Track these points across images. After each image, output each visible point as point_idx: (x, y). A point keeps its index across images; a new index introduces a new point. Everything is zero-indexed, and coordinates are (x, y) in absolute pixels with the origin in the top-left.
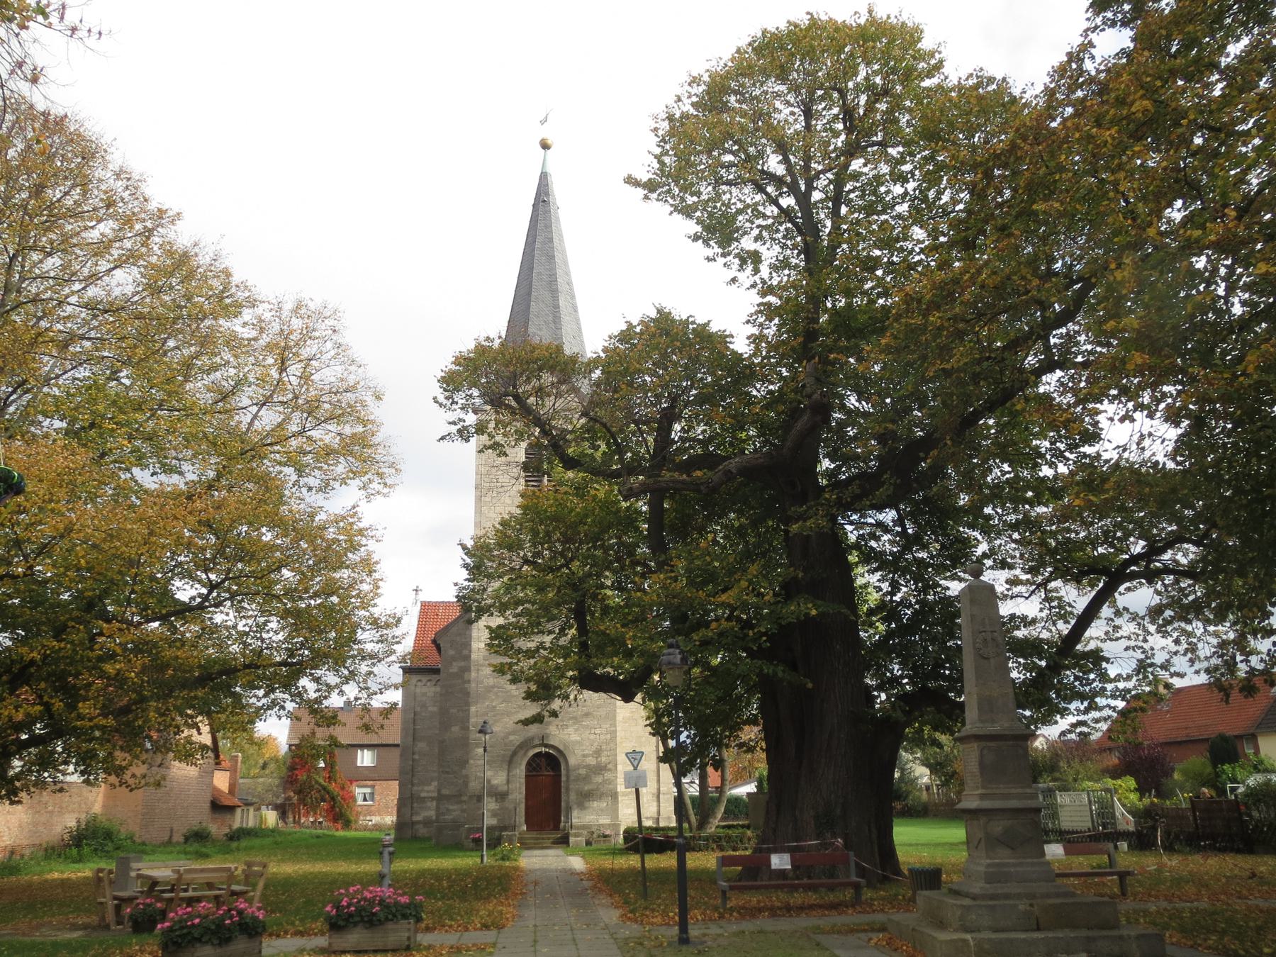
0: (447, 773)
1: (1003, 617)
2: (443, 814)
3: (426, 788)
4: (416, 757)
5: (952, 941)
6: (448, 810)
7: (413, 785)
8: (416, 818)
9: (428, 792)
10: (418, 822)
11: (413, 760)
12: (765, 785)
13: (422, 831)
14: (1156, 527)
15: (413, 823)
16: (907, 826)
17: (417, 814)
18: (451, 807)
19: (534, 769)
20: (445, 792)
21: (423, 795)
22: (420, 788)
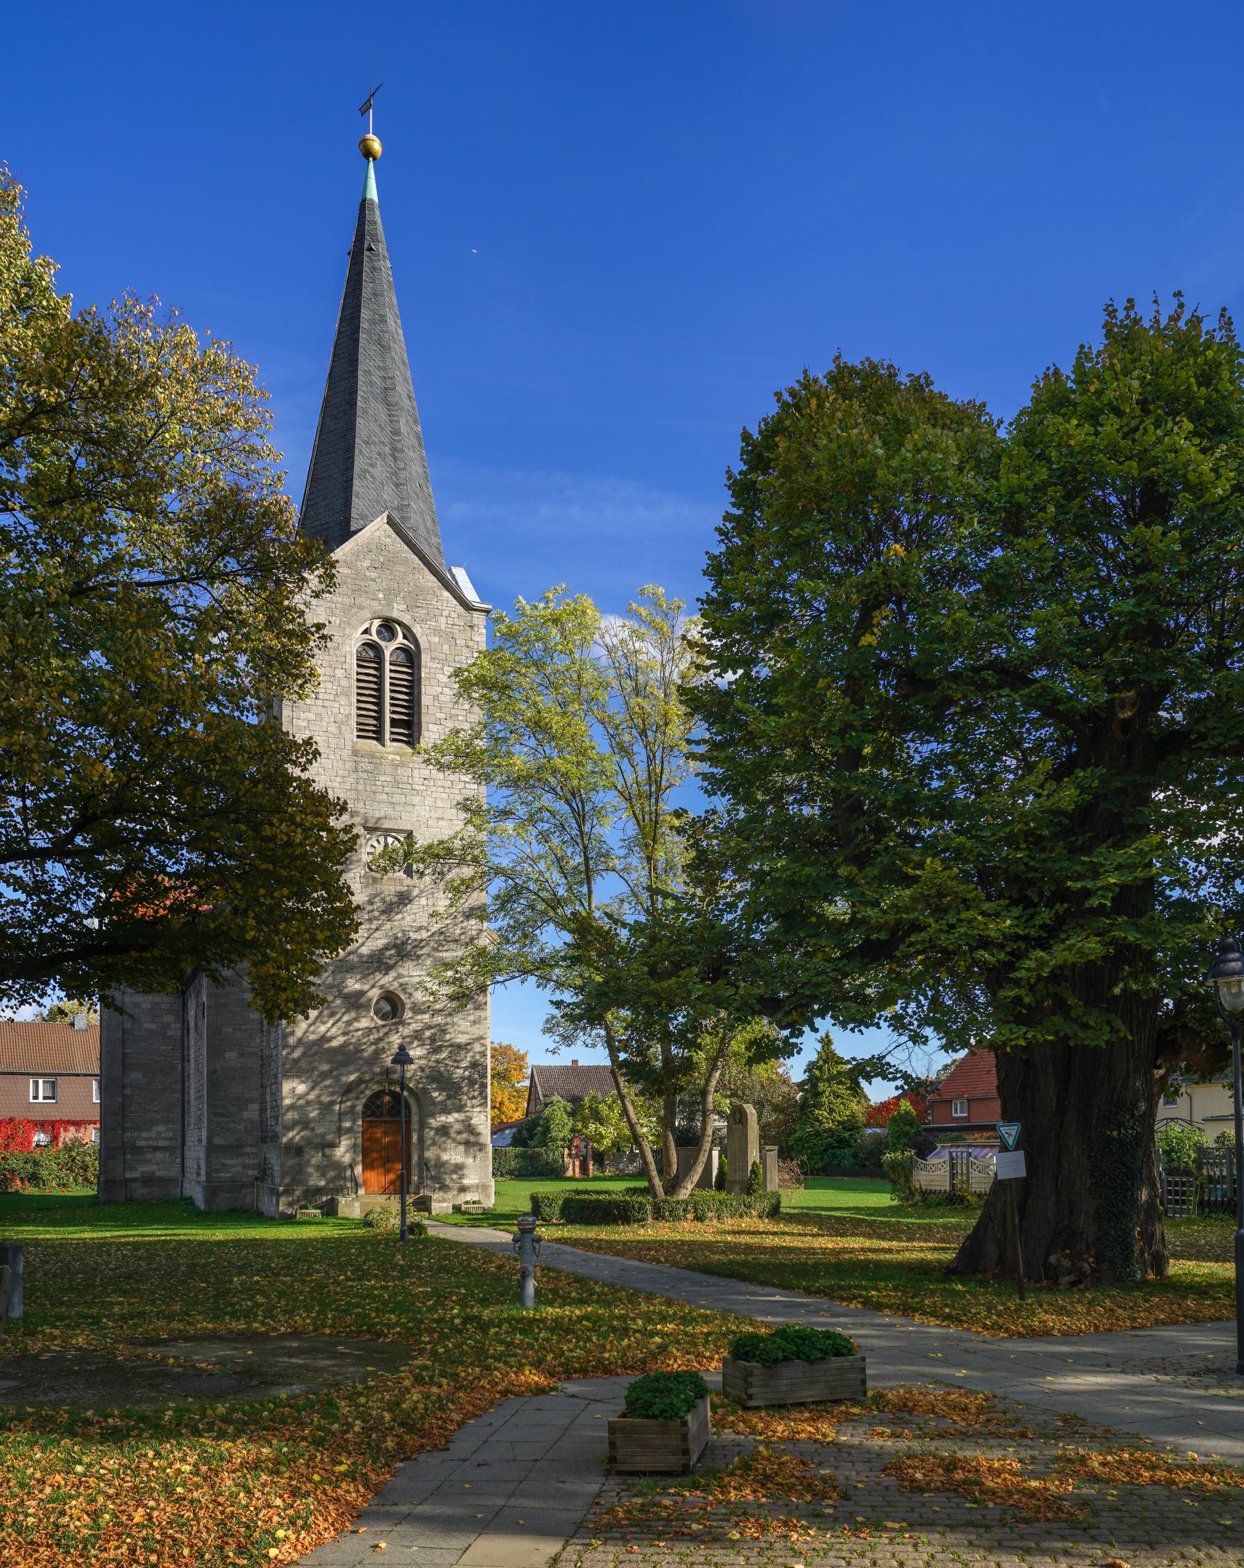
0: (221, 1115)
1: (840, 1061)
2: (217, 1171)
3: (144, 1134)
4: (128, 1091)
5: (676, 1146)
6: (223, 1165)
7: (124, 1129)
8: (128, 1175)
9: (148, 1139)
10: (135, 1180)
11: (124, 1096)
12: (847, 1256)
13: (140, 1191)
14: (81, 1463)
15: (128, 1181)
16: (854, 1190)
17: (132, 1169)
18: (228, 1162)
19: (373, 1114)
20: (218, 1141)
21: (140, 1143)
22: (135, 1135)
